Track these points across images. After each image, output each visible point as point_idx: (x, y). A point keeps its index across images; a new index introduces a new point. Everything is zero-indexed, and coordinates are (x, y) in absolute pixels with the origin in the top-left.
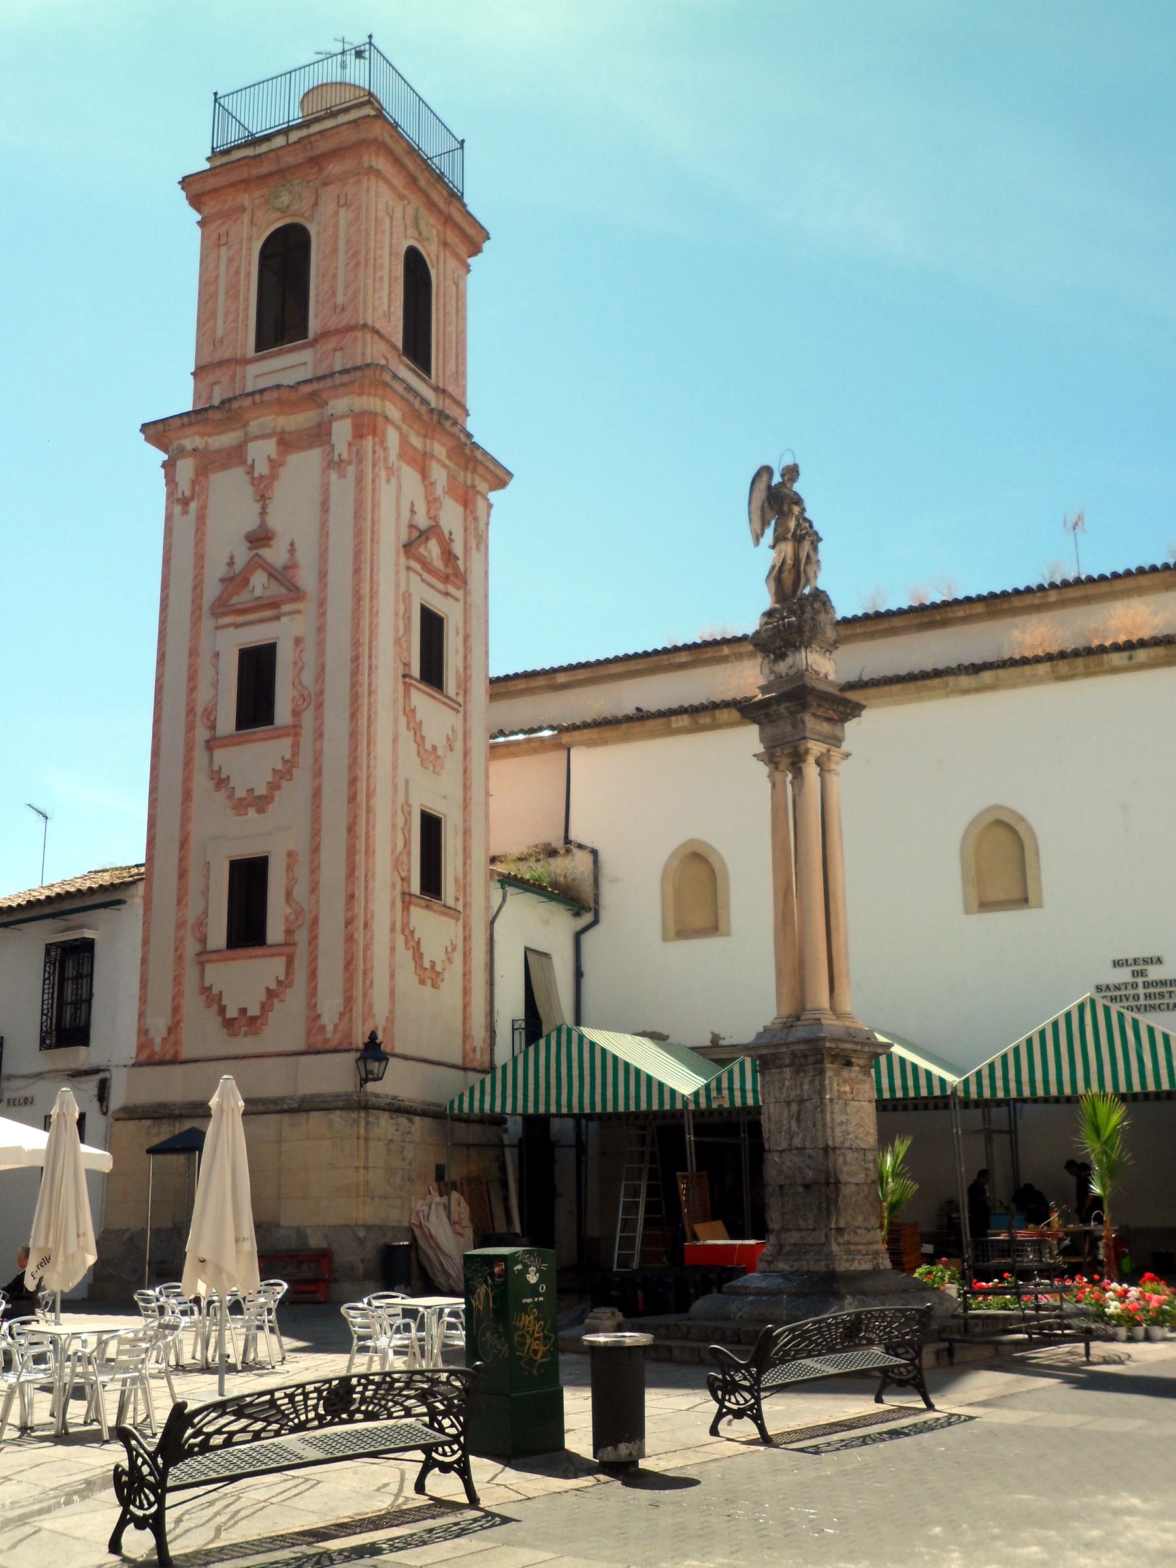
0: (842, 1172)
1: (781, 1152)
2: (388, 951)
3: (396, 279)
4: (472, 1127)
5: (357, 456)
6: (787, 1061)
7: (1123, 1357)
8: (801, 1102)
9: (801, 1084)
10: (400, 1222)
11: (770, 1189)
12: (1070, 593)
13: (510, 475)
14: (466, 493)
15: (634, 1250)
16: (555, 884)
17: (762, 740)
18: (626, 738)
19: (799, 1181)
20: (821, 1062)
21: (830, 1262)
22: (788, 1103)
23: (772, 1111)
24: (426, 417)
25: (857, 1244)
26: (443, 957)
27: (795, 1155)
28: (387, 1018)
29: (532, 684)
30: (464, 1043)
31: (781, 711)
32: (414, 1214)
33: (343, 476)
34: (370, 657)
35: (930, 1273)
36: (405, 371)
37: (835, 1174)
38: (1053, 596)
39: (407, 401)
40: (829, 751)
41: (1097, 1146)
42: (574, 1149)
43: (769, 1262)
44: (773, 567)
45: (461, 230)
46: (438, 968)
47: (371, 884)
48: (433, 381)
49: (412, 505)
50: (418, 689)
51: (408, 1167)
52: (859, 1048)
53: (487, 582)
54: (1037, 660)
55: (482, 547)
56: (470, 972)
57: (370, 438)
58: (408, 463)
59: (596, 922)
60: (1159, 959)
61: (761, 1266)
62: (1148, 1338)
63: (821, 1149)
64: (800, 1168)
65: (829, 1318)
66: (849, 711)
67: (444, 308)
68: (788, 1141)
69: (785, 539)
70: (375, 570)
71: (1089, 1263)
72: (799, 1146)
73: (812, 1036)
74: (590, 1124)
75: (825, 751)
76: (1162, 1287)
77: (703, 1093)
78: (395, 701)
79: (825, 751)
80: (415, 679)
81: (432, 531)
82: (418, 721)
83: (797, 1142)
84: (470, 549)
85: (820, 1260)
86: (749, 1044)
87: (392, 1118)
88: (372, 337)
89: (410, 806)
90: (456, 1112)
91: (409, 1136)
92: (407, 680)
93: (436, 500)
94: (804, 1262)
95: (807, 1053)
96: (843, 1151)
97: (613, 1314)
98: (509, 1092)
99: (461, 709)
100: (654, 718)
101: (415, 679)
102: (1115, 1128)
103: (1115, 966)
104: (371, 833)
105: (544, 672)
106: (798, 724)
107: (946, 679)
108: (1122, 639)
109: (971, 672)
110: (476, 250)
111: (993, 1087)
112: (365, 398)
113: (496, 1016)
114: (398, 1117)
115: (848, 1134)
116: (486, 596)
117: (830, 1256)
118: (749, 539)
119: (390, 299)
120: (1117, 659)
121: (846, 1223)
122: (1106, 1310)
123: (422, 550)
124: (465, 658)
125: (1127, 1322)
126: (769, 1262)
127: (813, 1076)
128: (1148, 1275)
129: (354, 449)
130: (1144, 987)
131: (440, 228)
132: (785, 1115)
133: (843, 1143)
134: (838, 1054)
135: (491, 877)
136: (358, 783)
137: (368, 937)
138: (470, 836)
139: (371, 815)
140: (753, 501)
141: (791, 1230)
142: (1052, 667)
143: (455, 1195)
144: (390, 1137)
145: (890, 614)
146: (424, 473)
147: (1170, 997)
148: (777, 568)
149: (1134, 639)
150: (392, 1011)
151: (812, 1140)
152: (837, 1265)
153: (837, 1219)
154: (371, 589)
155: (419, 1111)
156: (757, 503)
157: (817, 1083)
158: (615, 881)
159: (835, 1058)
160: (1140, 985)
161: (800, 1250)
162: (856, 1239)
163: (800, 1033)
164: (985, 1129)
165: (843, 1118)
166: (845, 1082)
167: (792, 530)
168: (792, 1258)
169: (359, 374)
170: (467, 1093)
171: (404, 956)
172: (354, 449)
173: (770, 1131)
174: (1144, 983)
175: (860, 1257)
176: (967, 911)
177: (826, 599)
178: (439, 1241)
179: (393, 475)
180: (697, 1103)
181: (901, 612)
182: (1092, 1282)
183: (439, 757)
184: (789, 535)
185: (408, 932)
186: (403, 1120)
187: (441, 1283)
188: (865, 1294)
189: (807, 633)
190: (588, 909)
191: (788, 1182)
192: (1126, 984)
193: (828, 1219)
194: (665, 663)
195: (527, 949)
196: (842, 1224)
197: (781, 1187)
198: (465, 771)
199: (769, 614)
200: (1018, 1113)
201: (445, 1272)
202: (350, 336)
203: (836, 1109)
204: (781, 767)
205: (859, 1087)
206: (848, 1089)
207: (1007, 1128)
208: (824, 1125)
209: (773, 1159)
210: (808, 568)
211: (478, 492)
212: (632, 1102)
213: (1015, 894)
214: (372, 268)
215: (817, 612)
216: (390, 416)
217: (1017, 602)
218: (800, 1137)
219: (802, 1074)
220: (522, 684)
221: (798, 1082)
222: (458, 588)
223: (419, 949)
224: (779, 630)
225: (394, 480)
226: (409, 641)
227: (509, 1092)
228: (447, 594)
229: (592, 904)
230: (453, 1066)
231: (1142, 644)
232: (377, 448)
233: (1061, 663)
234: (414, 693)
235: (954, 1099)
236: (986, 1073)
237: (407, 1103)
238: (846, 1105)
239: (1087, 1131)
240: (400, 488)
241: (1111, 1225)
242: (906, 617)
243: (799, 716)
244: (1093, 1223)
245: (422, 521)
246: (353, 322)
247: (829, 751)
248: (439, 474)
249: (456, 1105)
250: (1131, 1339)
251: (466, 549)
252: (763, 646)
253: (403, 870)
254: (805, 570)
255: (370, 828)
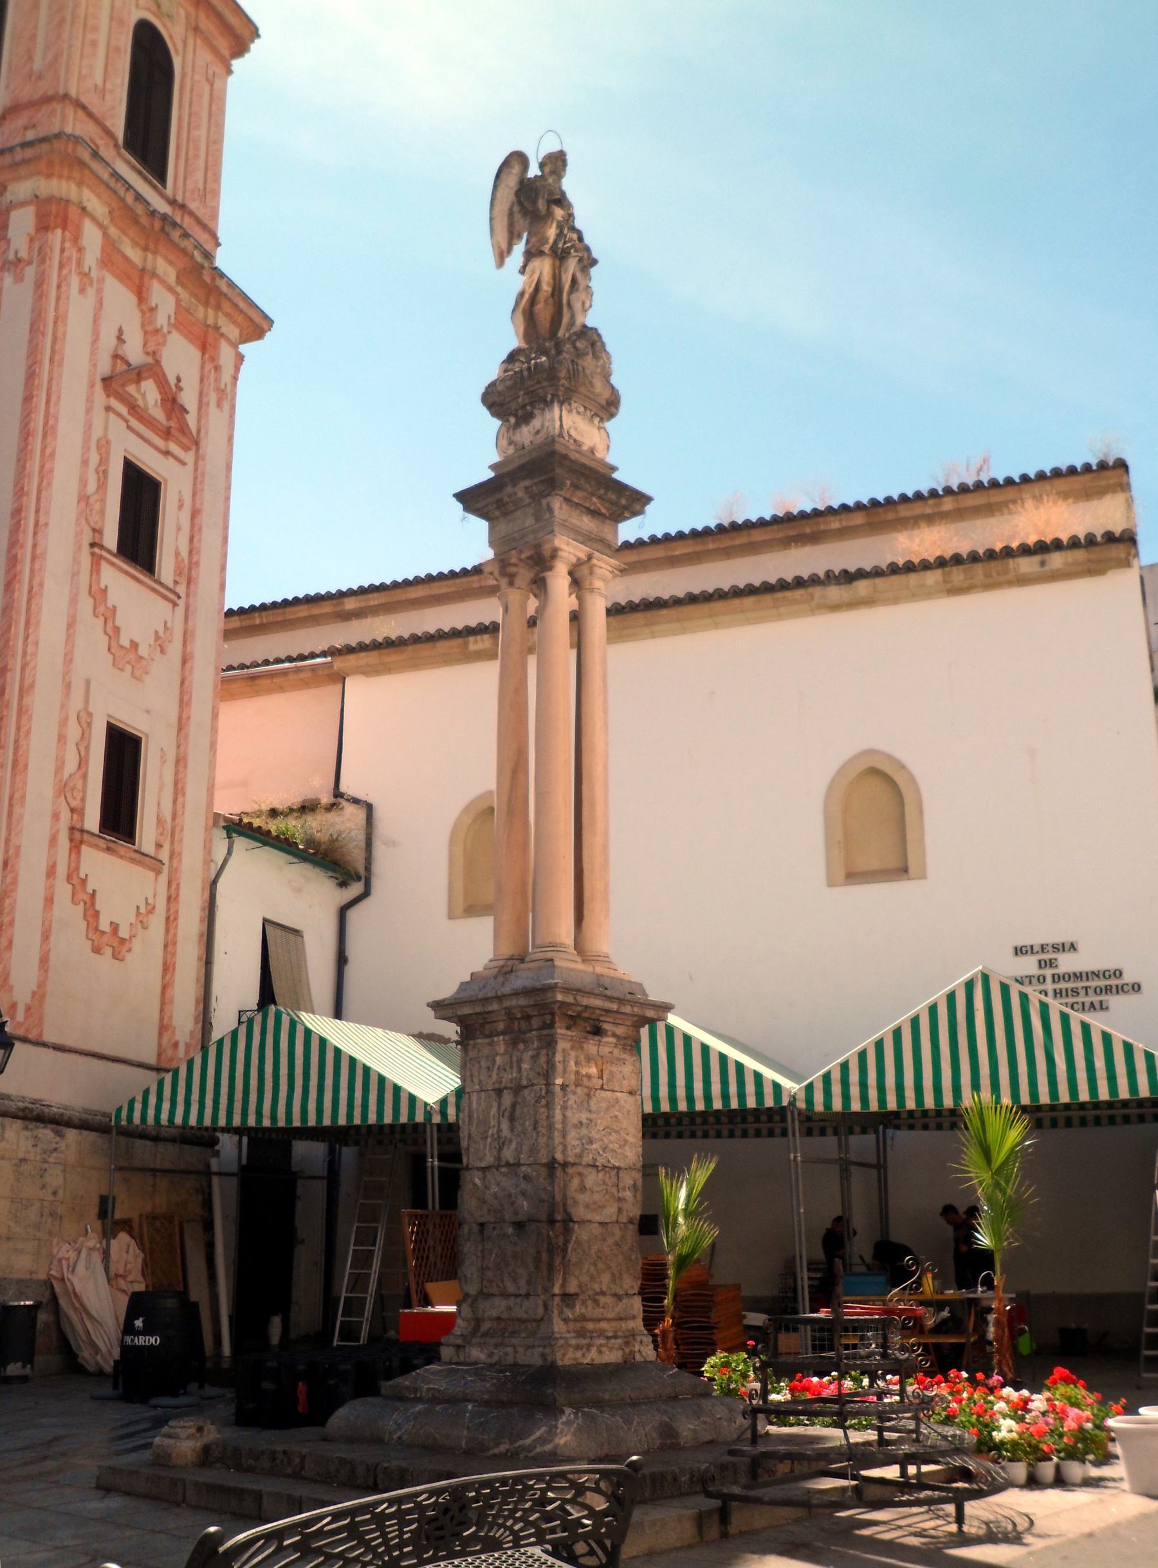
0: (576, 1202)
1: (484, 1170)
2: (40, 904)
3: (118, 50)
4: (161, 1146)
5: (39, 254)
6: (501, 1026)
7: (1022, 1524)
8: (518, 1089)
9: (520, 1061)
10: (31, 1273)
11: (466, 1229)
12: (970, 501)
13: (270, 322)
14: (206, 333)
15: (362, 1315)
16: (310, 842)
17: (492, 543)
18: (414, 665)
19: (507, 1217)
20: (551, 1026)
21: (547, 1350)
22: (499, 1092)
23: (474, 1105)
24: (144, 220)
25: (599, 1320)
26: (133, 919)
27: (504, 1175)
28: (34, 993)
29: (316, 610)
30: (160, 1034)
31: (520, 494)
32: (55, 1262)
33: (19, 279)
34: (37, 511)
35: (726, 1365)
36: (126, 168)
37: (565, 1205)
38: (948, 504)
39: (115, 192)
40: (590, 557)
41: (987, 1176)
42: (325, 1182)
43: (458, 1347)
44: (521, 294)
45: (219, 16)
46: (124, 933)
47: (17, 810)
48: (169, 191)
49: (121, 331)
50: (112, 564)
51: (51, 1198)
52: (614, 1007)
53: (231, 451)
54: (925, 566)
55: (226, 405)
56: (175, 944)
57: (59, 232)
58: (114, 274)
59: (366, 894)
60: (1072, 945)
61: (446, 1353)
62: (1060, 1482)
63: (544, 1165)
64: (510, 1196)
65: (381, 1502)
66: (624, 502)
67: (191, 106)
68: (495, 1153)
69: (541, 253)
70: (54, 399)
71: (974, 1343)
72: (512, 1161)
73: (538, 985)
74: (346, 1151)
75: (583, 556)
76: (1078, 1392)
77: (452, 1100)
78: (75, 575)
79: (583, 556)
80: (109, 552)
81: (153, 370)
82: (110, 605)
83: (508, 1154)
84: (208, 404)
85: (533, 1347)
86: (443, 1001)
87: (26, 1128)
88: (75, 113)
89: (90, 715)
90: (124, 1123)
91: (54, 1155)
92: (96, 550)
93: (157, 331)
94: (510, 1350)
95: (531, 1012)
96: (580, 1169)
97: (200, 1429)
98: (195, 1096)
99: (182, 603)
100: (446, 638)
101: (109, 552)
102: (1012, 1150)
103: (1017, 954)
104: (22, 742)
105: (328, 597)
106: (543, 516)
107: (810, 590)
108: (1031, 540)
109: (842, 581)
110: (240, 48)
111: (846, 1097)
112: (54, 182)
113: (213, 1004)
114: (37, 1128)
115: (591, 1142)
116: (229, 467)
117: (549, 1340)
118: (490, 257)
119: (106, 72)
120: (1026, 565)
121: (580, 1286)
122: (994, 1434)
123: (131, 389)
124: (191, 539)
125: (1026, 1453)
126: (458, 1347)
127: (538, 1048)
128: (1059, 1371)
129: (37, 245)
130: (1054, 981)
131: (192, 11)
132: (494, 1110)
133: (580, 1156)
134: (579, 1016)
135: (215, 824)
136: (9, 674)
137: (8, 880)
138: (186, 767)
139: (25, 718)
140: (497, 202)
141: (493, 1295)
142: (944, 575)
143: (123, 1238)
144: (21, 1155)
145: (748, 525)
146: (141, 294)
147: (1087, 994)
148: (527, 296)
149: (1048, 539)
150: (41, 985)
151: (531, 1150)
152: (559, 1355)
153: (565, 1280)
154: (46, 423)
155: (76, 1121)
156: (503, 206)
157: (543, 1059)
158: (392, 843)
159: (573, 1021)
160: (1049, 979)
161: (506, 1328)
162: (597, 1312)
163: (521, 980)
164: (840, 1158)
165: (584, 1117)
166: (589, 1059)
167: (551, 241)
168: (493, 1341)
169: (45, 147)
170: (139, 1098)
171: (68, 912)
172: (37, 245)
173: (470, 1137)
174: (1053, 975)
175: (602, 1341)
176: (831, 884)
177: (596, 338)
178: (85, 1301)
179: (91, 284)
180: (444, 1114)
181: (762, 523)
182: (973, 1382)
183: (141, 658)
184: (546, 248)
185: (79, 881)
186: (46, 1133)
187: (86, 1361)
188: (599, 1404)
189: (563, 381)
190: (359, 878)
191: (492, 1220)
192: (1030, 977)
193: (550, 1279)
194: (476, 585)
195: (266, 921)
196: (572, 1288)
197: (482, 1225)
198: (183, 682)
199: (512, 357)
200: (889, 1142)
201: (93, 1345)
202: (45, 109)
203: (570, 1103)
204: (518, 581)
205: (614, 1069)
206: (593, 1070)
207: (875, 1162)
208: (551, 1127)
209: (473, 1180)
210: (573, 296)
211: (222, 335)
212: (357, 1112)
213: (893, 862)
214: (81, 27)
215: (580, 354)
216: (89, 208)
217: (904, 511)
218: (514, 1145)
219: (521, 1046)
220: (302, 611)
221: (514, 1059)
222: (186, 449)
223: (93, 904)
224: (522, 375)
225: (91, 292)
226: (103, 501)
227: (195, 1096)
228: (167, 453)
229: (362, 872)
230: (140, 1065)
231: (1057, 545)
232: (67, 245)
233: (955, 569)
234: (104, 566)
235: (792, 1113)
236: (836, 1076)
237: (55, 1110)
238: (589, 1095)
239: (972, 1154)
240: (101, 304)
241: (1005, 1291)
242: (769, 528)
243: (544, 502)
244: (980, 1289)
245: (135, 353)
246: (51, 92)
247: (590, 557)
248: (164, 302)
249: (124, 1114)
250: (1033, 1482)
251: (202, 404)
252: (501, 405)
253: (74, 798)
254: (569, 301)
255: (22, 735)
